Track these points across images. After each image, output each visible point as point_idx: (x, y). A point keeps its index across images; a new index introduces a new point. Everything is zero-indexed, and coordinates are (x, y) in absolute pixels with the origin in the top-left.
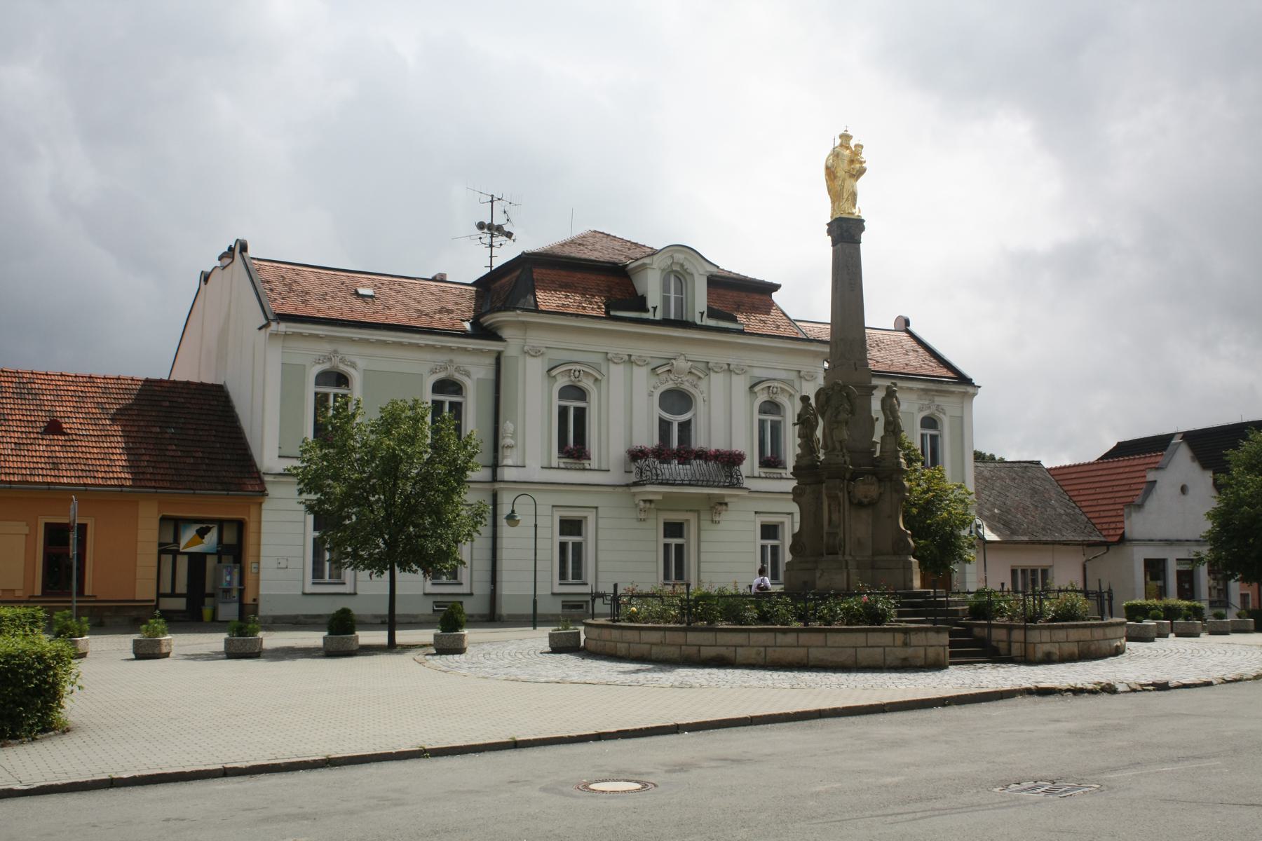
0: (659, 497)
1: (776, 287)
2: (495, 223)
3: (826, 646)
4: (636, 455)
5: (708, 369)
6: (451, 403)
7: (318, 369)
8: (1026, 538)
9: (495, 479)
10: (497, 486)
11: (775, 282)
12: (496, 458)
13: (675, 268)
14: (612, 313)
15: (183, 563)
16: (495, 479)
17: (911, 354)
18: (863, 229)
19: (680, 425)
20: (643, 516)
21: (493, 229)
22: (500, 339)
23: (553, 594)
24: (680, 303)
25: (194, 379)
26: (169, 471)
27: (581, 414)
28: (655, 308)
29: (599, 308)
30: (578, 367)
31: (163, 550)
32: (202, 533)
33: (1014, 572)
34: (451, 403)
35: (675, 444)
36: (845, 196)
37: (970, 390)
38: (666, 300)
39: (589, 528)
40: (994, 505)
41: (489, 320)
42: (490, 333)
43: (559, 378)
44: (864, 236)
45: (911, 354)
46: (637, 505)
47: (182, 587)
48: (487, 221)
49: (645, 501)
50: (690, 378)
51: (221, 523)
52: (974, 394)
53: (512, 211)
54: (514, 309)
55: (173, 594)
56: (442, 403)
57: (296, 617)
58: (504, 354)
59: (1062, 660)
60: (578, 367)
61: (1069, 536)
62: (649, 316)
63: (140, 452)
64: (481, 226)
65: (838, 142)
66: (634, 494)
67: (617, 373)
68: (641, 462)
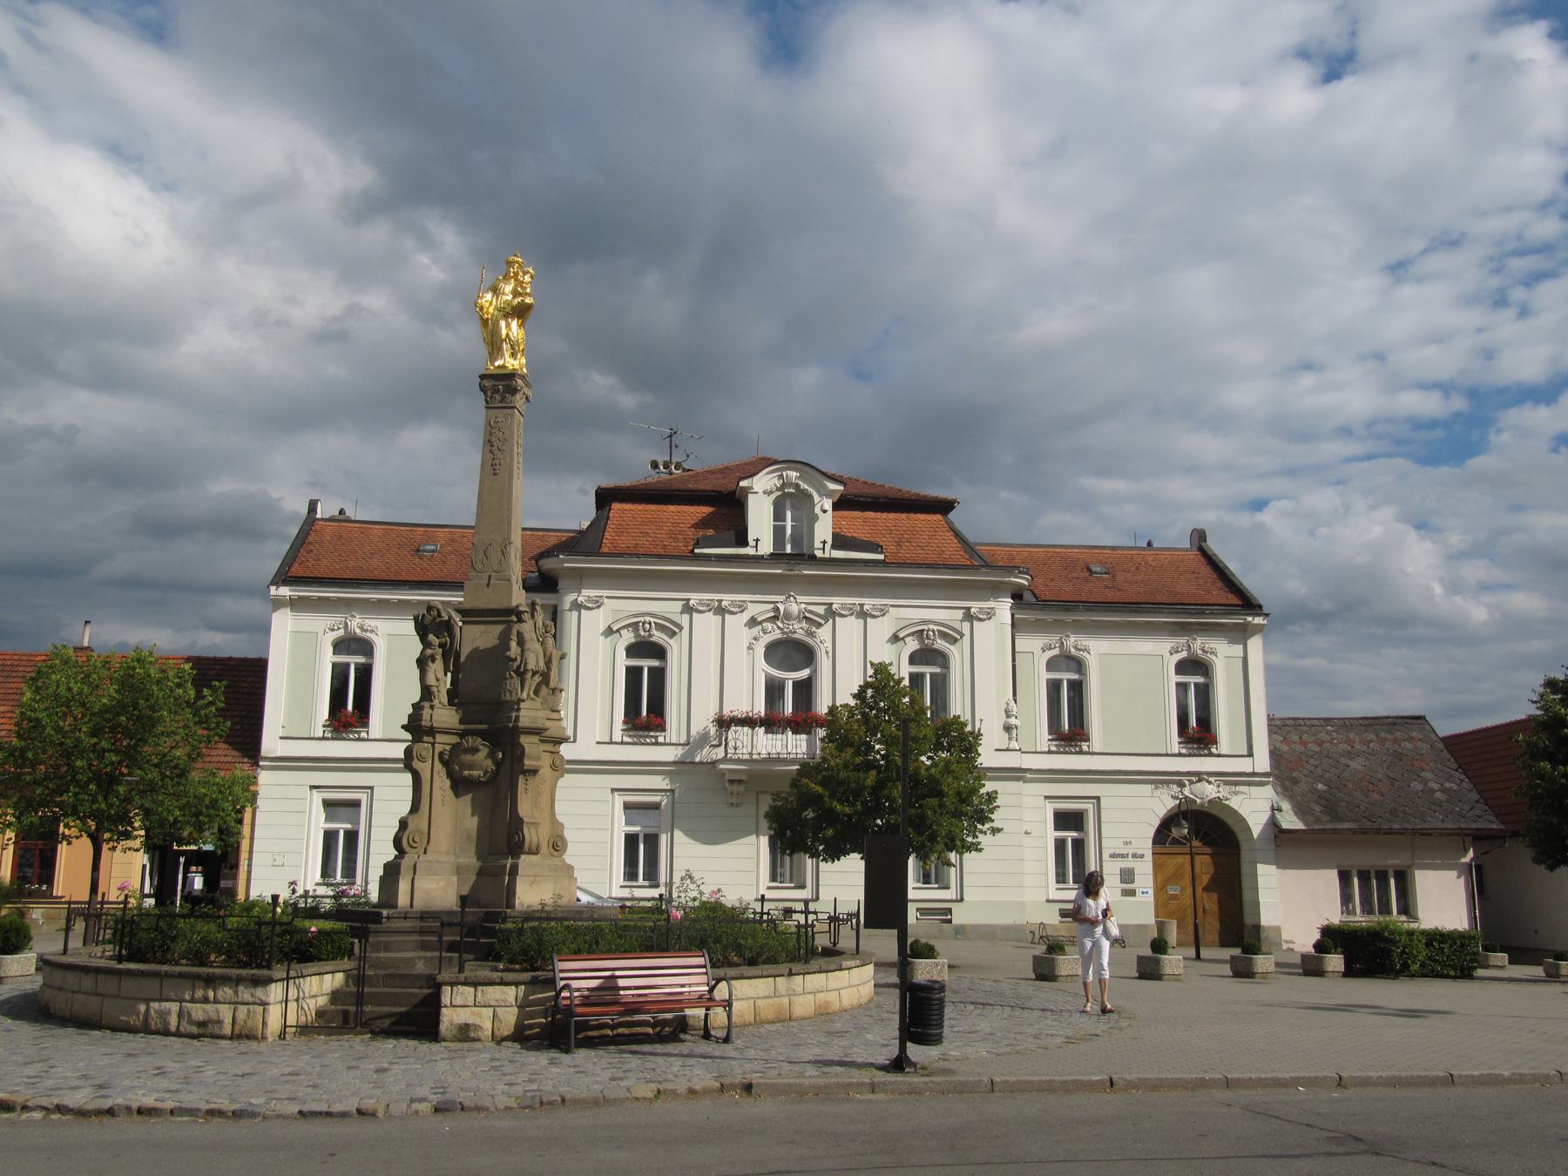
5: (831, 614)
7: (333, 636)
8: (1353, 826)
19: (796, 684)
20: (735, 801)
23: (1048, 901)
38: (779, 533)
40: (1320, 779)
43: (624, 632)
60: (648, 619)
62: (749, 551)
67: (706, 624)
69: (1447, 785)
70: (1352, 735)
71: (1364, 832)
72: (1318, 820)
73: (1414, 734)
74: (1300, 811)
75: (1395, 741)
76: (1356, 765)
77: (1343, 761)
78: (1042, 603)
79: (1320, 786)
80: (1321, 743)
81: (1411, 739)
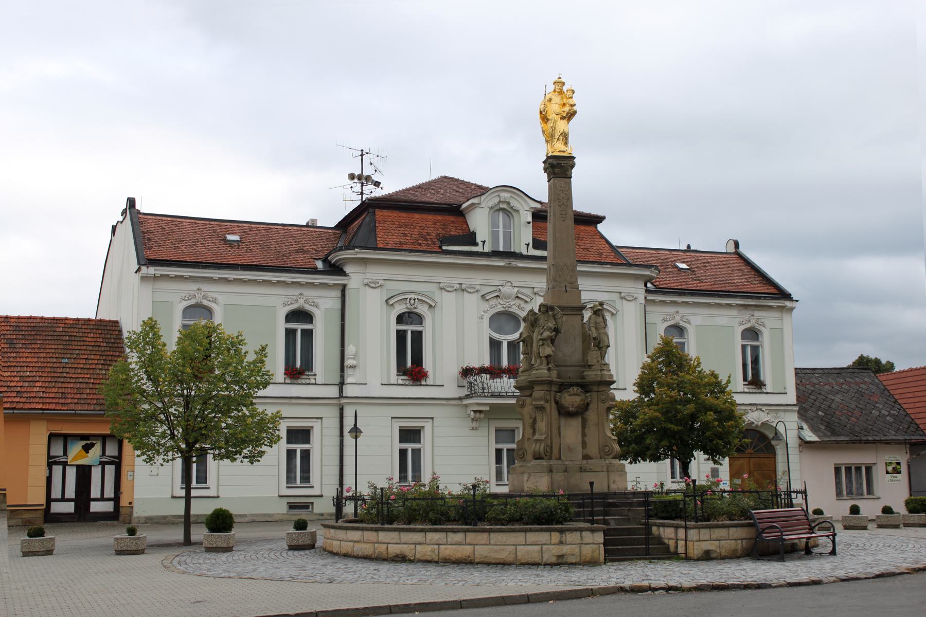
0: (487, 408)
1: (600, 219)
2: (365, 174)
3: (490, 544)
4: (467, 372)
6: (302, 330)
8: (847, 439)
9: (341, 396)
10: (343, 401)
11: (600, 214)
12: (342, 377)
13: (502, 206)
14: (444, 248)
15: (71, 474)
16: (341, 396)
17: (736, 273)
18: (573, 166)
21: (363, 179)
22: (343, 273)
24: (508, 237)
25: (107, 318)
26: (57, 395)
27: (418, 337)
28: (484, 242)
29: (434, 243)
30: (413, 296)
31: (52, 462)
32: (87, 448)
33: (837, 470)
34: (302, 330)
35: (505, 363)
36: (557, 137)
37: (788, 304)
38: (495, 235)
39: (426, 436)
40: (819, 409)
41: (334, 258)
42: (336, 269)
44: (574, 171)
45: (736, 273)
46: (469, 416)
47: (71, 492)
48: (357, 172)
49: (475, 412)
50: (518, 302)
51: (104, 438)
52: (792, 309)
53: (377, 163)
54: (353, 248)
55: (63, 499)
56: (295, 331)
57: (165, 517)
58: (348, 287)
59: (723, 558)
60: (413, 296)
61: (892, 436)
62: (478, 249)
63: (35, 379)
64: (352, 177)
65: (551, 88)
66: (466, 406)
67: (447, 301)
68: (472, 378)
69: (892, 412)
70: (830, 380)
71: (853, 442)
72: (825, 435)
73: (866, 379)
74: (814, 429)
75: (856, 384)
76: (838, 398)
77: (830, 396)
78: (659, 291)
79: (820, 413)
80: (814, 385)
81: (865, 383)
